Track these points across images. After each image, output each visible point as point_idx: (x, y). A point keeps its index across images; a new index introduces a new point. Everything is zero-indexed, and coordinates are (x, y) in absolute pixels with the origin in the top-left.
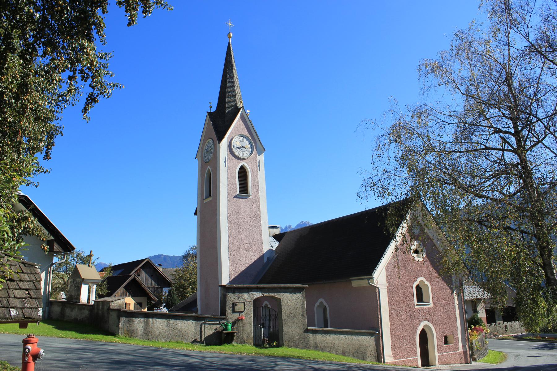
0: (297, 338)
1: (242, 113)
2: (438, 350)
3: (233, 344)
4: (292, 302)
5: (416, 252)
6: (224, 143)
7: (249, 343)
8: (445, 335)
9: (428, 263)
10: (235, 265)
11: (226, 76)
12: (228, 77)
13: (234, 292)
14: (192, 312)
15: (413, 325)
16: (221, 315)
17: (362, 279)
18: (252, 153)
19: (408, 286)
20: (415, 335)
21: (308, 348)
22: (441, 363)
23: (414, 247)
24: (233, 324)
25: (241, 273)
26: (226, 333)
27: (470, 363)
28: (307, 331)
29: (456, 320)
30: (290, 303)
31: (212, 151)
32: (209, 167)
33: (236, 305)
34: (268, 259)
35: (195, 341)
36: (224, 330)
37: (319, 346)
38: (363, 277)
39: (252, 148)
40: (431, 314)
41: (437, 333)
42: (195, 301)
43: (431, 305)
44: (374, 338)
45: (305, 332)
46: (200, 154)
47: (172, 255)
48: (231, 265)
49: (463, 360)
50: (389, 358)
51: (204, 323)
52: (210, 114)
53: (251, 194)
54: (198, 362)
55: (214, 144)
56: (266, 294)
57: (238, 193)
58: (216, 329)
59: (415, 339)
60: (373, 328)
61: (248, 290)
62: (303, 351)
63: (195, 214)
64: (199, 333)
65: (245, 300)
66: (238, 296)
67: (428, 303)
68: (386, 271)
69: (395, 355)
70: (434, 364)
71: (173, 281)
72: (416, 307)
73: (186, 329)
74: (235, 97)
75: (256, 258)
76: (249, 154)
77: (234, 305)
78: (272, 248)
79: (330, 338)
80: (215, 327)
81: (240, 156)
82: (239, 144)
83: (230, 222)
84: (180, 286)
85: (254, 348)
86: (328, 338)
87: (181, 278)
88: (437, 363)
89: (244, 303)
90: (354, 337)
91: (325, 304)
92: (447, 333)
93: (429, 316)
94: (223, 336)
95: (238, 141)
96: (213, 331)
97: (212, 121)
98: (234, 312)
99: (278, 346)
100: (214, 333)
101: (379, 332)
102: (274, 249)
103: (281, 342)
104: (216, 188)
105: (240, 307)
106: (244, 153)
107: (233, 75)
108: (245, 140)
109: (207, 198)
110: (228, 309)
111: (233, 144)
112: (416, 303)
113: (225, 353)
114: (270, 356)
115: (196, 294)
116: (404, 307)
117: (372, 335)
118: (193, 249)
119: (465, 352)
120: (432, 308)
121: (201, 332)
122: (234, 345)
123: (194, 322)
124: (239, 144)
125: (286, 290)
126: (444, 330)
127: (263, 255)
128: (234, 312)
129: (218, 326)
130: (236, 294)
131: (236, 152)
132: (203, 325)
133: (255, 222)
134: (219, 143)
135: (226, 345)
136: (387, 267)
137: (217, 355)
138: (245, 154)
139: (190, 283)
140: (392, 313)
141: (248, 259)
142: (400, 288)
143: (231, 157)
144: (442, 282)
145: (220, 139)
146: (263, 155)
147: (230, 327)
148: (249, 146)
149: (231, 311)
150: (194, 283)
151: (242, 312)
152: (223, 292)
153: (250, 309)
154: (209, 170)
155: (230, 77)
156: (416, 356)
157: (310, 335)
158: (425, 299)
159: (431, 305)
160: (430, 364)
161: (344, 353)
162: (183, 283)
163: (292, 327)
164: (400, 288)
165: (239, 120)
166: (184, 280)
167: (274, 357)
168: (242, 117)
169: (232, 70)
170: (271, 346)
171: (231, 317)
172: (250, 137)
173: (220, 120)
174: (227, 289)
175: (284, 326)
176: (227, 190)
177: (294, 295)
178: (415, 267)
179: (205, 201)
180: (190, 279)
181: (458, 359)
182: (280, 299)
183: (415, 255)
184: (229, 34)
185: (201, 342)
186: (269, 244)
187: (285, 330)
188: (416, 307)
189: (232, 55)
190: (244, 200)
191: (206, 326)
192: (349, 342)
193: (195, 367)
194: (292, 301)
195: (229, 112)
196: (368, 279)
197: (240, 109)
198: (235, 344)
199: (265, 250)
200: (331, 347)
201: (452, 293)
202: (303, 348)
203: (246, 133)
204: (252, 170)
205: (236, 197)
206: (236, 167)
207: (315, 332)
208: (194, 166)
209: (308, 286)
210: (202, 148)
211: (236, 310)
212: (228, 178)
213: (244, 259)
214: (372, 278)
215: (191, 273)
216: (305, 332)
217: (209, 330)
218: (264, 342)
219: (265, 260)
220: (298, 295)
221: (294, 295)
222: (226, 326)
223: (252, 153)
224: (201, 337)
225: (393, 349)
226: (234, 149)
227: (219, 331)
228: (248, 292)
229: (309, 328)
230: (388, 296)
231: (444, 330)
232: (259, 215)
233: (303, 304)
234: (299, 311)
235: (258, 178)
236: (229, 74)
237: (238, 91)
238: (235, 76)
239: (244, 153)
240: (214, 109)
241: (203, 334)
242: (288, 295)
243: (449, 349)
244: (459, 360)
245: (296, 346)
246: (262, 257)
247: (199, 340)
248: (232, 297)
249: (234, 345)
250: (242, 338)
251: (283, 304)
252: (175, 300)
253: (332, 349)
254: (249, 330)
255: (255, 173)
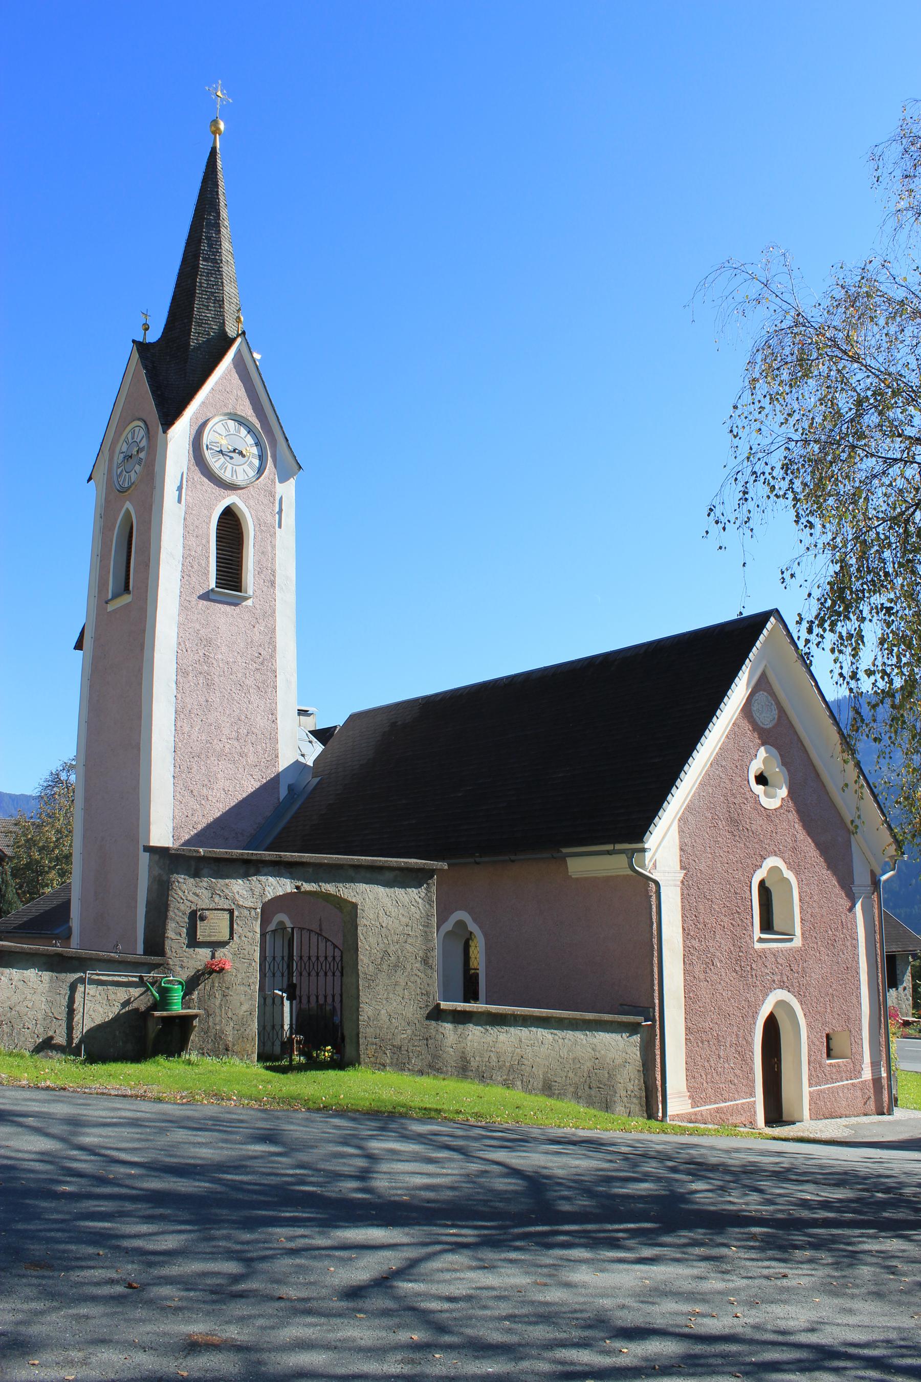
0: (403, 1036)
1: (239, 352)
2: (810, 1075)
3: (185, 1056)
4: (391, 915)
5: (761, 779)
6: (180, 432)
7: (242, 1055)
8: (828, 1030)
9: (793, 816)
10: (192, 803)
11: (200, 241)
12: (204, 247)
13: (196, 874)
14: (49, 938)
15: (747, 1000)
16: (146, 953)
17: (609, 853)
18: (260, 471)
19: (739, 881)
20: (751, 1032)
21: (439, 1070)
22: (817, 1115)
23: (756, 766)
24: (191, 985)
25: (209, 826)
26: (163, 1019)
27: (890, 1113)
28: (436, 1014)
29: (859, 988)
30: (385, 920)
31: (142, 455)
32: (128, 505)
33: (203, 919)
34: (291, 788)
35: (45, 1046)
36: (155, 1006)
37: (474, 1064)
38: (609, 847)
39: (262, 458)
40: (795, 967)
41: (809, 1025)
42: (65, 906)
43: (797, 942)
44: (637, 1038)
45: (429, 1017)
46: (103, 468)
47: (18, 793)
48: (178, 801)
49: (872, 1104)
50: (678, 1102)
51: (82, 981)
52: (142, 347)
53: (250, 592)
54: (45, 1157)
55: (149, 434)
56: (307, 887)
57: (213, 584)
58: (127, 1003)
59: (750, 1044)
60: (637, 1011)
61: (248, 868)
62: (426, 1082)
63: (79, 646)
64: (63, 1016)
65: (234, 901)
66: (211, 888)
67: (788, 935)
68: (681, 831)
69: (695, 1094)
70: (796, 1117)
71: (8, 852)
72: (758, 946)
73: (15, 999)
74: (221, 306)
75: (257, 785)
76: (252, 473)
77: (195, 917)
78: (301, 759)
79: (508, 1040)
80: (122, 994)
81: (227, 476)
82: (224, 442)
83: (182, 671)
84: (28, 866)
85: (258, 1069)
86: (502, 1037)
87: (31, 843)
88: (806, 1113)
89: (231, 912)
90: (579, 1035)
91: (472, 927)
92: (835, 1025)
93: (791, 974)
94: (153, 1029)
95: (220, 433)
96: (116, 1009)
97: (145, 367)
98: (193, 942)
99: (340, 1063)
100: (117, 1019)
101: (654, 1020)
102: (310, 763)
103: (349, 1050)
104: (147, 565)
105: (216, 926)
106: (239, 470)
107: (218, 242)
108: (243, 432)
109: (116, 596)
110: (175, 934)
111: (206, 438)
112: (757, 933)
113: (159, 1100)
114: (324, 1110)
115: (67, 888)
116: (726, 945)
117: (633, 1029)
118: (68, 768)
119: (877, 1081)
120: (799, 950)
121: (71, 1012)
122: (189, 1063)
123: (47, 975)
124: (225, 444)
125: (373, 875)
126: (829, 1017)
127: (278, 776)
128: (193, 942)
129: (135, 992)
130: (205, 882)
131: (216, 463)
132: (80, 988)
133: (258, 676)
134: (165, 432)
135: (161, 1059)
136: (683, 820)
137: (127, 1110)
138: (240, 471)
139: (57, 859)
140: (691, 964)
141: (232, 785)
142: (716, 887)
143: (198, 476)
144: (826, 874)
145: (169, 417)
146: (292, 482)
147: (177, 994)
148: (255, 450)
149: (184, 940)
150: (68, 857)
151: (223, 944)
152: (157, 871)
153: (250, 934)
154: (128, 513)
155: (210, 246)
156: (752, 1094)
157: (447, 1027)
158: (778, 922)
159: (797, 942)
160: (785, 1117)
161: (548, 1089)
162: (37, 856)
163: (387, 1003)
164: (716, 887)
165: (228, 371)
166: (41, 850)
167: (342, 1113)
168: (240, 365)
169: (217, 226)
170: (314, 1065)
171: (185, 960)
172: (258, 426)
173: (172, 368)
174: (170, 861)
175: (363, 998)
176: (178, 575)
177: (399, 893)
178: (758, 824)
179: (110, 607)
180: (56, 847)
181: (860, 1102)
182: (354, 906)
183: (759, 789)
184: (215, 122)
185: (69, 1049)
186: (295, 748)
187: (367, 1010)
188: (758, 946)
189: (221, 183)
190: (228, 608)
191: (91, 989)
192: (564, 1053)
193: (27, 1193)
194: (394, 911)
195: (199, 347)
196: (631, 854)
197: (233, 340)
198: (194, 1057)
199: (283, 763)
200: (511, 1069)
201: (851, 909)
202: (421, 1073)
203: (247, 411)
204: (259, 523)
205: (206, 596)
206: (210, 508)
207: (461, 1018)
208: (85, 502)
209: (445, 866)
210: (112, 451)
211: (200, 937)
212: (184, 537)
213: (220, 784)
214: (644, 850)
215: (59, 831)
216: (429, 1017)
217: (99, 1005)
218: (287, 1047)
219: (283, 793)
220: (413, 892)
221: (399, 892)
222: (165, 992)
223: (260, 471)
224: (70, 1029)
225: (691, 1075)
226: (207, 454)
227: (137, 1010)
228: (246, 875)
229: (444, 1005)
230: (683, 908)
231: (829, 1017)
232: (273, 656)
233: (427, 925)
234: (414, 947)
235: (274, 547)
236: (209, 238)
237: (230, 290)
238: (226, 245)
239: (239, 470)
240: (154, 336)
241: (77, 1018)
242: (380, 890)
243: (840, 1075)
244: (861, 1105)
245: (401, 1066)
246: (273, 784)
247: (60, 1040)
248: (189, 892)
249: (189, 1063)
250: (219, 1037)
251: (361, 922)
252: (10, 904)
253: (512, 1074)
254: (245, 1007)
255: (268, 532)
